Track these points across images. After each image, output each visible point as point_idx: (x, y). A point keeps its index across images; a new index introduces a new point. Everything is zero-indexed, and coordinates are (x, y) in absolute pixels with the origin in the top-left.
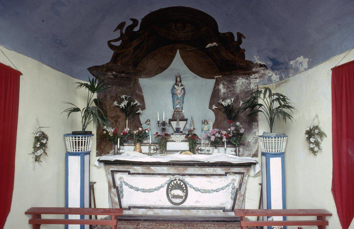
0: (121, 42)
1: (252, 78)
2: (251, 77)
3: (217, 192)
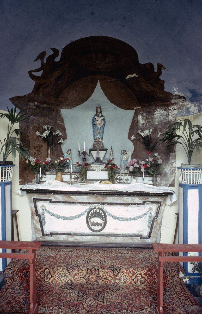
1: (170, 110)
2: (170, 108)
3: (134, 220)
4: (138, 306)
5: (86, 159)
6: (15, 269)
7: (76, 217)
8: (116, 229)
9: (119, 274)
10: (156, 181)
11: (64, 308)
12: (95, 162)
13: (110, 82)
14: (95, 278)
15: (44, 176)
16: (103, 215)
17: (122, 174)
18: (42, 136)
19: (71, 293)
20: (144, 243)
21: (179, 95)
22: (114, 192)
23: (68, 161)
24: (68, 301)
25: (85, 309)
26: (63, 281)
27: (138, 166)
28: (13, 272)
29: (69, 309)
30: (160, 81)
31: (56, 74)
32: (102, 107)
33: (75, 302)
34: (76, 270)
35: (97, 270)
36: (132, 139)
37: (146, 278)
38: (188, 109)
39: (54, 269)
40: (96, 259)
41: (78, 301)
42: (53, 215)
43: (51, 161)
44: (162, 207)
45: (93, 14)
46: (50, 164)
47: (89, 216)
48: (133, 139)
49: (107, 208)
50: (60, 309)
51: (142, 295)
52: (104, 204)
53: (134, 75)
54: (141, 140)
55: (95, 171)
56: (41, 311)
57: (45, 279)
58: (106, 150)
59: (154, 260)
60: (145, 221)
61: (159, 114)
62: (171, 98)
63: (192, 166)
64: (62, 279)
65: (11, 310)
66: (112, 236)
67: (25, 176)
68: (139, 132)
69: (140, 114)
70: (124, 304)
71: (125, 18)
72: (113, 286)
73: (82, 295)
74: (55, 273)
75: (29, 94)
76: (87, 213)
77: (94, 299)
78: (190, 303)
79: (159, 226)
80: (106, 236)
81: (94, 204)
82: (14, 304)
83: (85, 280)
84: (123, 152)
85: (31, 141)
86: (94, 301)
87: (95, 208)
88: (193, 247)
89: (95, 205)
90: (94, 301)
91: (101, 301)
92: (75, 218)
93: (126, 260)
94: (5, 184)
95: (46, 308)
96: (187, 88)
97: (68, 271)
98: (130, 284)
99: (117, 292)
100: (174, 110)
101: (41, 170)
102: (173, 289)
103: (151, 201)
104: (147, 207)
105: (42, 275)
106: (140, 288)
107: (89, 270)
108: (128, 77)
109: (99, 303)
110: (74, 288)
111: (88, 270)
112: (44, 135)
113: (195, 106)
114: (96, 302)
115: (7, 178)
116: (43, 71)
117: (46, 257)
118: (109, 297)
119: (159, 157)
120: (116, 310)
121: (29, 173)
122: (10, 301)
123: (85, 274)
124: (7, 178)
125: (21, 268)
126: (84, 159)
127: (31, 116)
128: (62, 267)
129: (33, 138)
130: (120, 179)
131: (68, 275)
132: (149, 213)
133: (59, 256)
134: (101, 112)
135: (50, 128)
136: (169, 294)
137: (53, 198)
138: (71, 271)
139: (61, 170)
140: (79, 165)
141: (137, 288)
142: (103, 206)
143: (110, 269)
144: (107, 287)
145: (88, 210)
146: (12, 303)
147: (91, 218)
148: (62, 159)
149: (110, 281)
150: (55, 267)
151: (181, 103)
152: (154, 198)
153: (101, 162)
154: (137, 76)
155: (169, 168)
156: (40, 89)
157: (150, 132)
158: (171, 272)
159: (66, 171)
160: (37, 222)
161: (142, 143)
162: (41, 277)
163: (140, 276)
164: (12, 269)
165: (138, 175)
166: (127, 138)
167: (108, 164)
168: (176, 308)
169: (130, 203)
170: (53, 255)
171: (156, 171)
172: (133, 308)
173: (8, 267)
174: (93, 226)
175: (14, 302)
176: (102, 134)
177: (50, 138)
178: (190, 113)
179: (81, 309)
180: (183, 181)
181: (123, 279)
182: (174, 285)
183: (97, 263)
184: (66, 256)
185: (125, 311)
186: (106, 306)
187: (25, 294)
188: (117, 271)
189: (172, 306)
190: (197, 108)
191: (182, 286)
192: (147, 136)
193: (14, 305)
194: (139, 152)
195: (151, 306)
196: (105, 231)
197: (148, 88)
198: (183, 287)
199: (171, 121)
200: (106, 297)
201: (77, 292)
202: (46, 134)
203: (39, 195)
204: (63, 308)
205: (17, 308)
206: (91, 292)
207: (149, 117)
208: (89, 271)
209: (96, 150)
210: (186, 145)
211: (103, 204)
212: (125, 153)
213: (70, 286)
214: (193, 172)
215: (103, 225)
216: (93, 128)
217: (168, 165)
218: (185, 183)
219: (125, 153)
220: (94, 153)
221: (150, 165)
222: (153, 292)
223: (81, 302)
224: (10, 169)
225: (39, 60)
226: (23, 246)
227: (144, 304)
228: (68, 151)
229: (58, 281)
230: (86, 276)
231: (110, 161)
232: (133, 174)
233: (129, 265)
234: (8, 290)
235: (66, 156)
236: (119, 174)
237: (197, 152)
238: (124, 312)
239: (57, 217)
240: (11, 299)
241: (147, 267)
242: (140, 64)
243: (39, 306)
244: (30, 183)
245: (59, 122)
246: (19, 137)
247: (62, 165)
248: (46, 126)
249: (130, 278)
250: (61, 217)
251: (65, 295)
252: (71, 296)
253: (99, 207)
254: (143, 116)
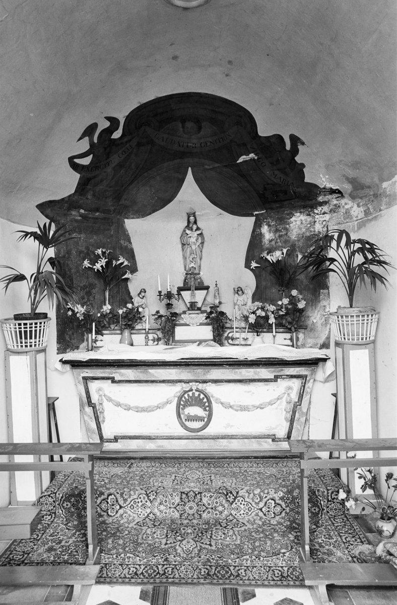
1: (318, 214)
2: (316, 211)
3: (261, 408)
4: (269, 549)
5: (173, 305)
6: (58, 496)
7: (158, 407)
8: (228, 425)
9: (237, 500)
10: (298, 339)
11: (144, 555)
12: (189, 309)
13: (210, 169)
14: (195, 508)
15: (99, 337)
16: (206, 403)
17: (237, 330)
18: (94, 267)
19: (154, 533)
20: (280, 449)
21: (331, 189)
22: (222, 360)
23: (140, 309)
24: (150, 545)
25: (180, 555)
26: (140, 515)
27: (263, 314)
28: (54, 501)
29: (153, 557)
30: (297, 165)
32: (196, 214)
33: (163, 546)
34: (161, 495)
35: (199, 493)
36: (251, 268)
37: (284, 506)
38: (347, 212)
39: (124, 495)
40: (196, 478)
41: (166, 544)
42: (118, 405)
43: (111, 311)
44: (309, 385)
45: (175, 58)
46: (111, 316)
47: (182, 405)
48: (255, 267)
49: (211, 389)
50: (138, 556)
51: (275, 531)
52: (207, 382)
53: (252, 155)
54: (269, 268)
55: (188, 325)
56: (106, 560)
57: (109, 511)
58: (207, 288)
59: (298, 476)
60: (280, 409)
61: (298, 223)
62: (317, 194)
63: (356, 309)
64: (138, 511)
65: (56, 559)
66: (222, 438)
67: (67, 338)
68: (264, 254)
69: (265, 222)
70: (246, 546)
71: (230, 62)
72: (225, 520)
73: (174, 535)
74: (125, 500)
75: (70, 196)
76: (176, 399)
77: (194, 541)
78: (357, 543)
79: (305, 418)
80: (212, 439)
81: (188, 383)
82: (60, 551)
83: (178, 511)
84: (237, 291)
85: (74, 277)
86: (194, 544)
87: (191, 390)
88: (357, 443)
89: (191, 384)
90: (194, 544)
91: (206, 544)
92: (156, 409)
93: (248, 478)
94: (36, 351)
95: (114, 556)
96: (344, 176)
97: (148, 497)
98: (255, 517)
99: (234, 529)
100: (324, 213)
101: (95, 327)
102: (330, 523)
103: (288, 373)
104: (283, 384)
105: (103, 506)
106: (274, 522)
107: (185, 495)
108: (241, 160)
109: (203, 546)
110: (159, 525)
111: (183, 494)
112: (98, 266)
113: (358, 206)
114: (198, 545)
115: (39, 341)
117: (108, 476)
118: (219, 537)
119: (300, 297)
120: (232, 556)
121: (73, 334)
122: (53, 546)
123: (177, 502)
124: (39, 341)
125: (67, 494)
126: (169, 306)
127: (73, 233)
128: (137, 490)
129: (78, 271)
130: (233, 339)
131: (148, 504)
132: (286, 395)
133: (131, 475)
134: (195, 222)
135: (107, 252)
136: (323, 530)
137: (118, 374)
138: (154, 497)
139: (129, 325)
140: (161, 316)
141: (268, 522)
142: (205, 385)
143: (220, 491)
144: (216, 522)
145: (179, 394)
146: (55, 550)
147: (185, 406)
148: (130, 306)
149: (221, 513)
150: (125, 492)
151: (335, 202)
152: (293, 369)
153: (199, 309)
154: (256, 158)
155: (319, 316)
156: (89, 187)
157: (283, 254)
158: (326, 493)
159: (138, 327)
160: (91, 418)
161: (270, 274)
162: (101, 509)
163: (273, 502)
164: (52, 497)
165: (265, 330)
166: (244, 265)
167: (211, 313)
168: (335, 550)
169: (253, 378)
170: (120, 474)
171: (295, 322)
172: (262, 552)
173: (46, 494)
174: (188, 421)
175: (60, 548)
176: (198, 260)
177: (107, 271)
178: (351, 219)
179: (173, 556)
180: (341, 335)
181: (244, 509)
182: (332, 515)
183: (198, 484)
184: (144, 474)
185: (248, 557)
186: (214, 551)
187: (76, 536)
188: (233, 495)
189: (327, 547)
190: (362, 209)
191: (346, 517)
192: (278, 261)
193: (59, 553)
194: (266, 289)
195: (292, 548)
196: (210, 430)
197: (276, 177)
198: (347, 519)
199: (319, 232)
200: (215, 538)
201: (165, 531)
202: (101, 264)
203: (93, 370)
204: (142, 556)
205: (66, 557)
206: (189, 531)
207: (280, 227)
208: (184, 496)
209: (189, 289)
210: (345, 276)
211: (205, 382)
212: (240, 293)
213: (153, 523)
214: (362, 320)
215: (206, 420)
216: (183, 250)
217: (316, 311)
218: (345, 338)
219: (240, 293)
220: (186, 295)
221: (285, 311)
222: (296, 528)
223: (173, 545)
224: (44, 326)
225: (87, 138)
226: (209, 144)
227: (279, 547)
228: (141, 291)
229: (131, 514)
230: (178, 505)
231: (214, 307)
232: (257, 328)
233: (253, 484)
234: (48, 531)
235: (137, 301)
236: (232, 330)
237: (361, 285)
238: (246, 559)
239: (126, 408)
240: (54, 544)
241: (284, 486)
242: (260, 137)
243: (101, 553)
244: (76, 351)
245: (122, 242)
246: (55, 271)
247: (131, 316)
248: (101, 249)
249: (255, 506)
250: (133, 407)
251: (145, 536)
252: (156, 537)
253: (197, 388)
254: (269, 226)
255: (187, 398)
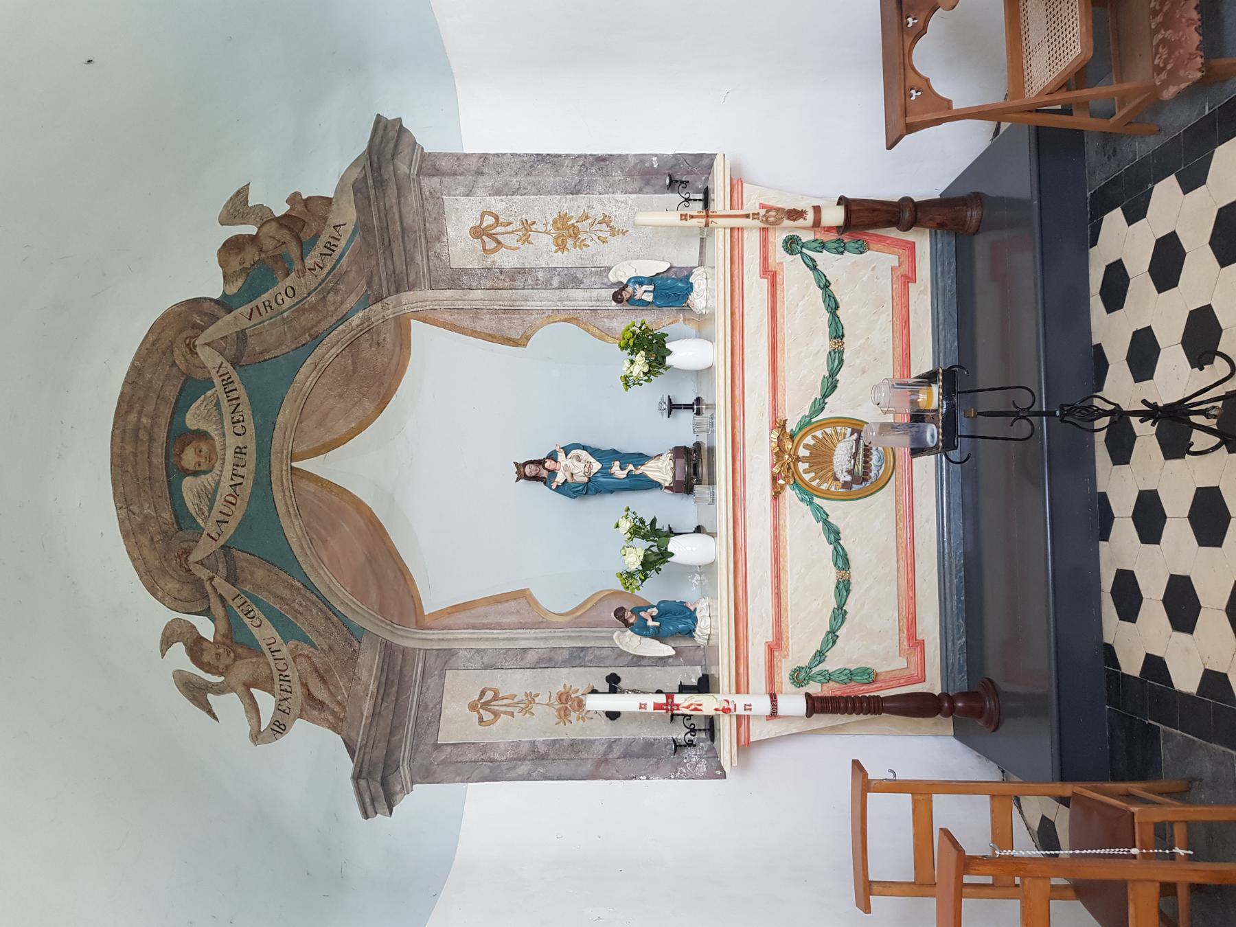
0: (256, 690)
3: (837, 307)
31: (265, 633)
116: (253, 687)
134: (540, 463)
226: (237, 417)
255: (818, 481)
